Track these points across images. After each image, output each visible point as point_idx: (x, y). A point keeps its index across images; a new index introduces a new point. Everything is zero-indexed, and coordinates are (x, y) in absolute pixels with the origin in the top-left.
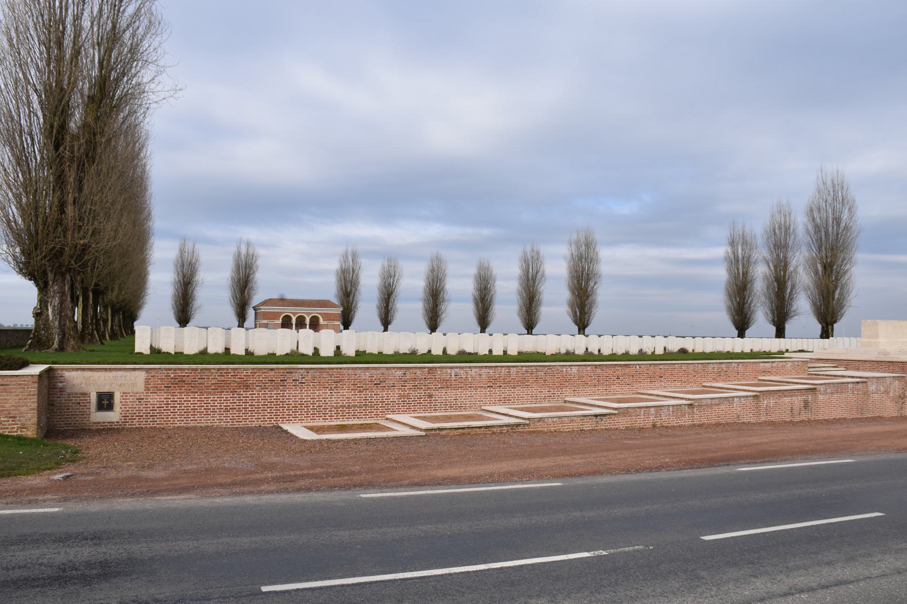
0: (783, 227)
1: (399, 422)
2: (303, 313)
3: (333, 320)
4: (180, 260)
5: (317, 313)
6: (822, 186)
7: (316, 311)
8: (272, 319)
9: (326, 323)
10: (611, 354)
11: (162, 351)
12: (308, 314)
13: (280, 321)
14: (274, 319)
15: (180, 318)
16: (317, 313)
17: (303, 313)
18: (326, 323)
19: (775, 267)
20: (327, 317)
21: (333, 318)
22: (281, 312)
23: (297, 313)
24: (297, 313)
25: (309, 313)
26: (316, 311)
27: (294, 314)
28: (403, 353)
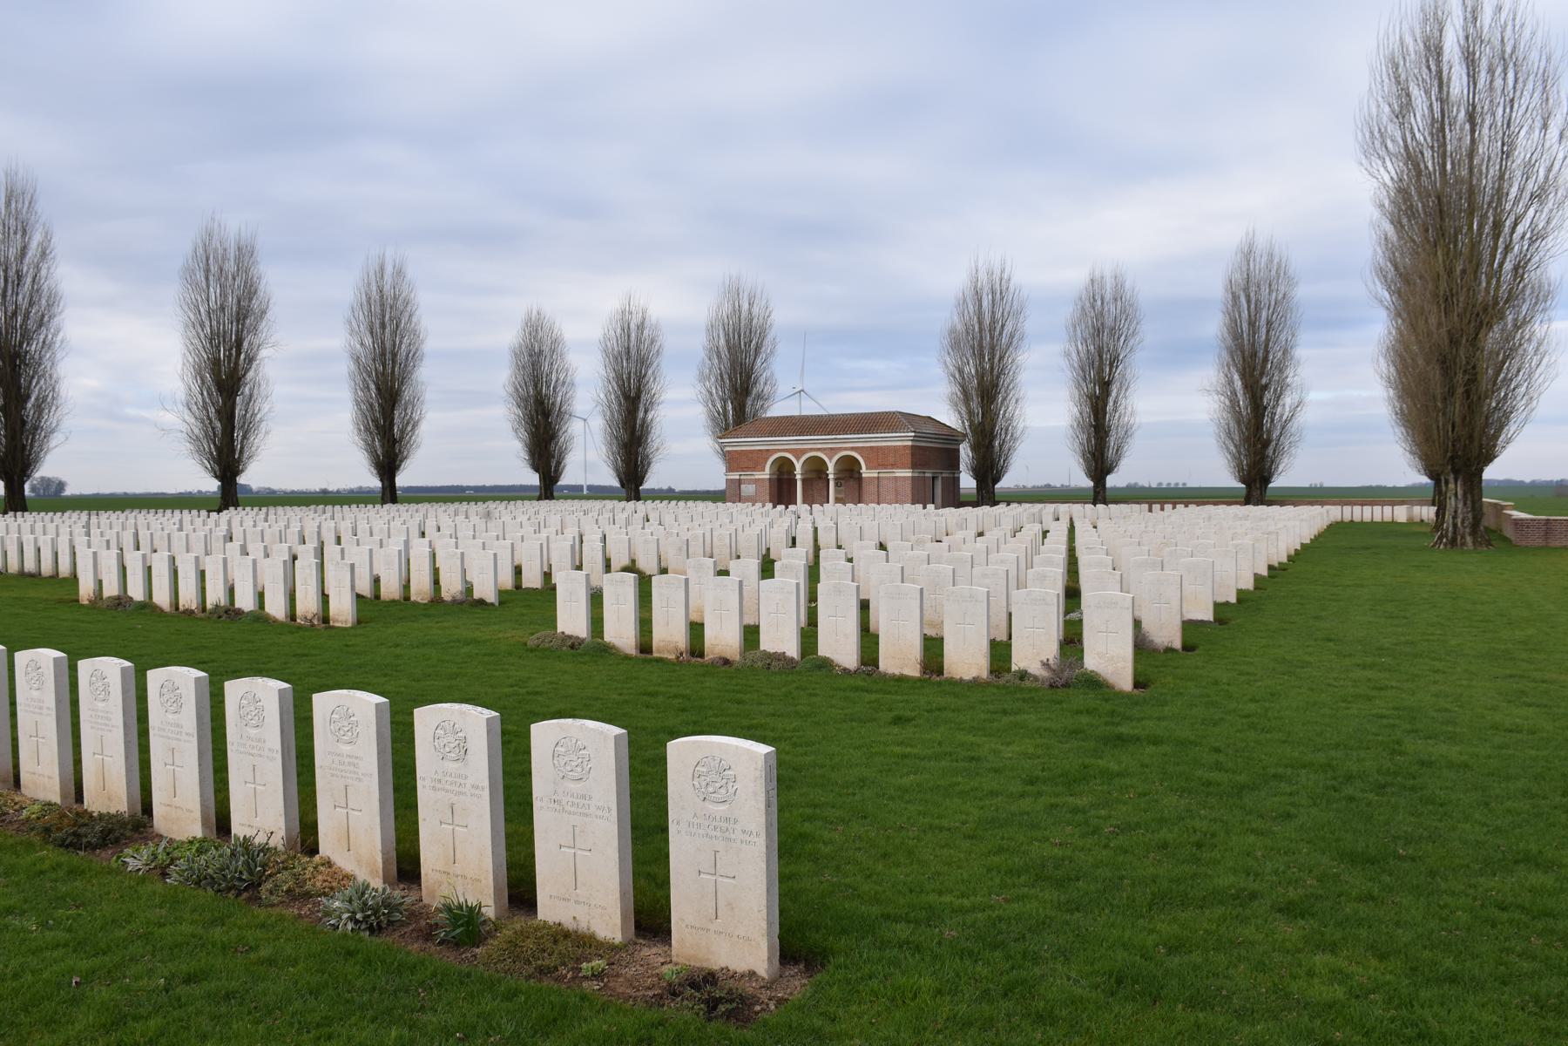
0: (1098, 298)
1: (321, 567)
2: (819, 450)
3: (894, 466)
4: (359, 413)
5: (852, 449)
6: (535, 313)
7: (850, 444)
8: (748, 469)
9: (874, 474)
10: (1337, 523)
11: (68, 492)
12: (833, 451)
13: (765, 474)
14: (754, 469)
15: (1426, 455)
16: (852, 449)
17: (819, 450)
18: (874, 474)
19: (1409, 313)
20: (879, 457)
21: (891, 460)
22: (768, 450)
23: (804, 451)
24: (804, 451)
25: (831, 449)
26: (850, 444)
27: (798, 453)
28: (1290, 558)
